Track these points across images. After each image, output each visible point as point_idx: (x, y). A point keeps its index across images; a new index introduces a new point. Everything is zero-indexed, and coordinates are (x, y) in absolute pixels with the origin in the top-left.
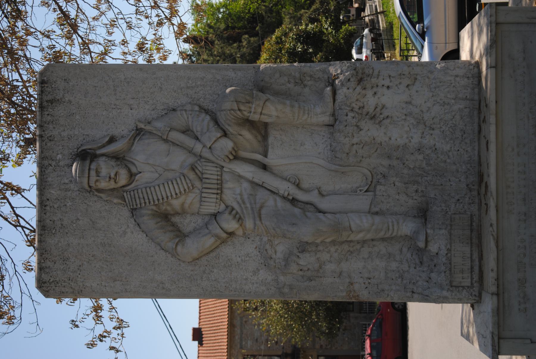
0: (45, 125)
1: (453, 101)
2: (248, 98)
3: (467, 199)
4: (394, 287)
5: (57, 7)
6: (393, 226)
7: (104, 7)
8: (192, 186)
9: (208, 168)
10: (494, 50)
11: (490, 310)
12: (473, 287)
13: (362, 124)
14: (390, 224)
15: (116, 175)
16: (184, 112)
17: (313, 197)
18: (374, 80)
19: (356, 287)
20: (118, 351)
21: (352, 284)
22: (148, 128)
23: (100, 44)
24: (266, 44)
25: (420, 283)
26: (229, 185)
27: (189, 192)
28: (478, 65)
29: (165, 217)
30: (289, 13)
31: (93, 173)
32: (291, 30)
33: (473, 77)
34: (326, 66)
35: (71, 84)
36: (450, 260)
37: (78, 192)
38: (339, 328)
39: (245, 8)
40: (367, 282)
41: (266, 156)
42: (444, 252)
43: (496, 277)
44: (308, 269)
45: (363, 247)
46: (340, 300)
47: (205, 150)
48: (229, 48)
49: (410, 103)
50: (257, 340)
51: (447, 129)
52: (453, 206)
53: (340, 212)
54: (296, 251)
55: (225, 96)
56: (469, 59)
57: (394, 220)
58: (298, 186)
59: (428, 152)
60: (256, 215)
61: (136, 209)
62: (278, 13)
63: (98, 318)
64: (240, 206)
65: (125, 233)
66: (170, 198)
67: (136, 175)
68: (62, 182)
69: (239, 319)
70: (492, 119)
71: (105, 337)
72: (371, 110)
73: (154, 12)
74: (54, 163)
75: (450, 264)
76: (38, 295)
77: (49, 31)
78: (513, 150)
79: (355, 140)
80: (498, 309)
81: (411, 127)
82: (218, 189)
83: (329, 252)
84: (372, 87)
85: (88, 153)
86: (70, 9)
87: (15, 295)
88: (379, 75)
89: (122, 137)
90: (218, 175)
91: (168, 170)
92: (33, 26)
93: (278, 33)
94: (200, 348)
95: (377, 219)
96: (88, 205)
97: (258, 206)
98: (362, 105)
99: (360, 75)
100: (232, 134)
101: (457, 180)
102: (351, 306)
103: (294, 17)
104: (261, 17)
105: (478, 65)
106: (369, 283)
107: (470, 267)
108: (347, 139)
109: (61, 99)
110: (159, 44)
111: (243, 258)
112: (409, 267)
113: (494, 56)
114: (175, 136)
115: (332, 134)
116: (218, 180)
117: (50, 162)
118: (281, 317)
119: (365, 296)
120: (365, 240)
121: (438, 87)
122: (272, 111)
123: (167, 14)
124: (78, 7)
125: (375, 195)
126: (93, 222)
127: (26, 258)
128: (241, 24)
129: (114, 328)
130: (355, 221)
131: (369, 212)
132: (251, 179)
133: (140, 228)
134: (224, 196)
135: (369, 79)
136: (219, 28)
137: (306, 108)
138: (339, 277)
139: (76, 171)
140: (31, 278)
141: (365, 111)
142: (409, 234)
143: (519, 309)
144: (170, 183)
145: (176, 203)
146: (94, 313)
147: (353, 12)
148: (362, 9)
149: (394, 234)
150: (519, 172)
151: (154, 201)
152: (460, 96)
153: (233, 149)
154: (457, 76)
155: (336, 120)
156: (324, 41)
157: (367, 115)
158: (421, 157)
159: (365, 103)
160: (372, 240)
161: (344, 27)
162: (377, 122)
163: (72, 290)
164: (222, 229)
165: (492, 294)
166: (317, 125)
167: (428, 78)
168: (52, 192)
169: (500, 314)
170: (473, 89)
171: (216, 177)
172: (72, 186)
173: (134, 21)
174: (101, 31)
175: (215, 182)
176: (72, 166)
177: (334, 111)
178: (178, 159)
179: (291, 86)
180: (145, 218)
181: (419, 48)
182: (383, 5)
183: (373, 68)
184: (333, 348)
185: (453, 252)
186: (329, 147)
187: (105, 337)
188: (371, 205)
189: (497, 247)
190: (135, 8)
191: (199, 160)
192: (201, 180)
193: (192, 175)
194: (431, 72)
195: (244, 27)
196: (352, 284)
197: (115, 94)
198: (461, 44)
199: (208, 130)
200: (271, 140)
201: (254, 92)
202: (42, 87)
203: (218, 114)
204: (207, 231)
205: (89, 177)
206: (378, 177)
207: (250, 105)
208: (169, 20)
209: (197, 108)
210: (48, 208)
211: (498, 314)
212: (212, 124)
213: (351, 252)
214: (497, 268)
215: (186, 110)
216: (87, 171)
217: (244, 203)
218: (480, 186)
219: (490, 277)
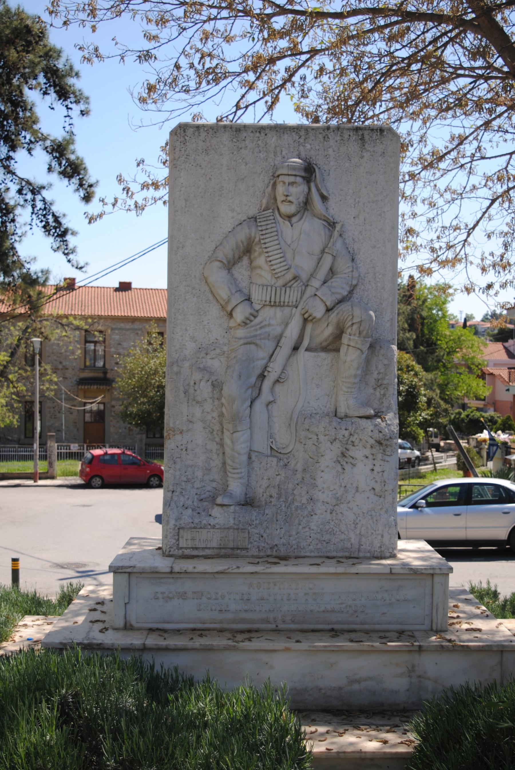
0: (339, 133)
1: (358, 532)
2: (364, 333)
3: (263, 545)
4: (178, 473)
5: (449, 149)
6: (238, 473)
7: (448, 196)
8: (278, 277)
9: (296, 292)
10: (408, 572)
11: (156, 565)
12: (178, 550)
13: (337, 444)
14: (239, 471)
15: (290, 202)
16: (351, 269)
17: (266, 396)
18: (380, 456)
19: (178, 437)
20: (114, 205)
21: (181, 433)
22: (336, 234)
23: (414, 190)
24: (407, 356)
25: (182, 498)
26: (279, 313)
27: (272, 274)
28: (393, 556)
29: (247, 250)
30: (436, 378)
31: (292, 179)
32: (420, 380)
33: (381, 551)
34: (394, 409)
35: (380, 158)
36: (204, 528)
37: (273, 164)
38: (131, 424)
39: (442, 336)
40: (183, 447)
41: (307, 350)
42: (212, 522)
43: (188, 571)
44: (196, 391)
45: (217, 444)
46: (165, 421)
47: (314, 290)
48: (403, 320)
49: (357, 491)
50: (120, 344)
51: (331, 526)
52: (256, 531)
53: (251, 422)
54: (213, 378)
55: (367, 310)
56: (399, 547)
57: (243, 474)
58: (277, 381)
59: (309, 508)
60: (249, 340)
61: (256, 221)
62: (437, 368)
63: (145, 186)
64: (258, 324)
65: (233, 210)
66: (267, 255)
67: (290, 221)
68: (283, 149)
69: (140, 327)
70: (340, 569)
71: (127, 193)
72: (351, 453)
73: (444, 245)
74: (302, 140)
75: (201, 528)
76: (173, 124)
77: (425, 141)
78: (311, 589)
79: (321, 437)
80: (157, 573)
81: (334, 492)
82: (275, 302)
83: (212, 411)
84: (373, 455)
85: (312, 174)
86: (447, 162)
87: (168, 105)
88: (384, 461)
89: (327, 209)
90: (289, 302)
91: (294, 253)
92: (432, 125)
93: (418, 368)
94: (112, 290)
95: (244, 458)
96: (260, 174)
97: (258, 342)
98: (356, 444)
99: (385, 443)
100: (329, 317)
101: (282, 536)
102: (152, 436)
103: (432, 383)
104: (433, 352)
105: (393, 556)
106: (182, 450)
107: (197, 546)
108: (323, 430)
109: (365, 148)
110: (411, 250)
111: (207, 327)
112: (197, 488)
113: (402, 571)
114: (328, 261)
115: (328, 415)
116: (284, 302)
117: (303, 137)
118: (142, 368)
119: (169, 446)
120: (223, 446)
121: (372, 518)
122: (351, 355)
123: (441, 257)
124: (448, 171)
125: (267, 456)
126: (243, 179)
127: (205, 115)
128: (426, 332)
129: (136, 202)
130: (242, 437)
131: (251, 450)
132: (285, 335)
133: (237, 225)
134: (268, 308)
135: (381, 451)
136: (422, 310)
137: (353, 390)
138: (188, 420)
139: (294, 162)
140: (187, 119)
141: (350, 447)
142: (229, 488)
143: (157, 593)
144: (282, 255)
145: (261, 261)
146: (150, 182)
147: (436, 441)
148: (438, 448)
149: (229, 474)
150: (289, 594)
151: (263, 239)
152: (363, 539)
153: (314, 318)
154: (382, 536)
155: (341, 419)
156: (409, 412)
157: (346, 449)
158: (304, 501)
159: (357, 447)
160: (224, 453)
161: (422, 431)
162: (339, 459)
163: (177, 158)
164: (236, 306)
165: (172, 567)
166: (336, 401)
167: (381, 509)
168: (274, 139)
169: (153, 574)
170: (369, 552)
171: (287, 300)
172: (279, 158)
173: (434, 225)
174: (427, 193)
175: (282, 300)
176: (299, 158)
177: (350, 417)
178: (304, 264)
179: (375, 375)
180: (247, 231)
181: (402, 503)
182: (443, 469)
183: (391, 455)
184: (112, 418)
185: (212, 530)
186: (315, 412)
187: (127, 193)
188: (258, 452)
189: (217, 573)
190: (448, 225)
191: (304, 284)
192: (284, 286)
193: (289, 276)
194: (386, 512)
195: (423, 335)
196: (181, 433)
197: (369, 202)
198: (411, 541)
199: (333, 293)
200: (323, 355)
201: (370, 339)
202: (377, 130)
203: (349, 303)
204: (234, 292)
205: (288, 175)
206: (285, 460)
207: (357, 335)
208: (435, 260)
209: (355, 282)
210: (258, 134)
211: (153, 572)
212: (339, 297)
213: (212, 433)
214: (197, 573)
215: (352, 271)
216: (294, 173)
217: (261, 328)
218: (276, 557)
219: (188, 565)
